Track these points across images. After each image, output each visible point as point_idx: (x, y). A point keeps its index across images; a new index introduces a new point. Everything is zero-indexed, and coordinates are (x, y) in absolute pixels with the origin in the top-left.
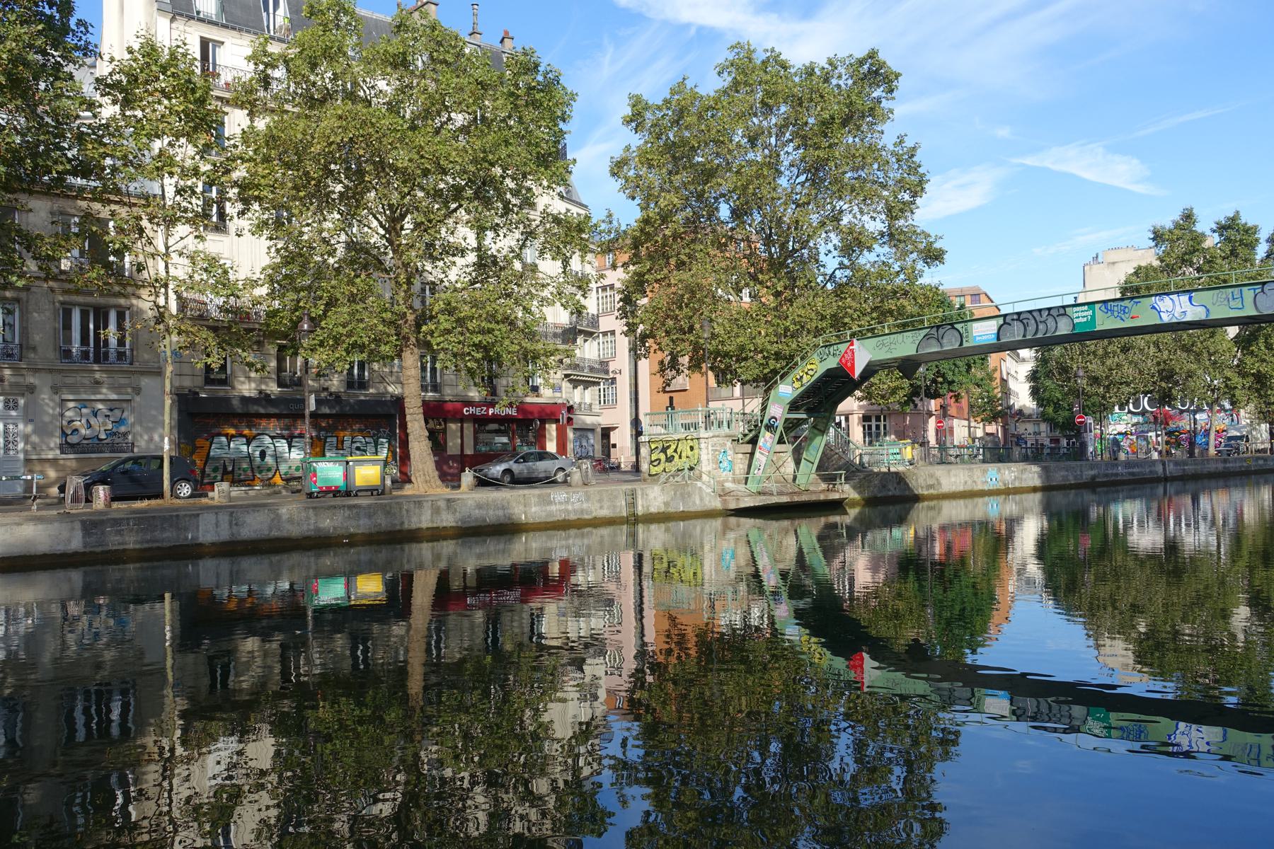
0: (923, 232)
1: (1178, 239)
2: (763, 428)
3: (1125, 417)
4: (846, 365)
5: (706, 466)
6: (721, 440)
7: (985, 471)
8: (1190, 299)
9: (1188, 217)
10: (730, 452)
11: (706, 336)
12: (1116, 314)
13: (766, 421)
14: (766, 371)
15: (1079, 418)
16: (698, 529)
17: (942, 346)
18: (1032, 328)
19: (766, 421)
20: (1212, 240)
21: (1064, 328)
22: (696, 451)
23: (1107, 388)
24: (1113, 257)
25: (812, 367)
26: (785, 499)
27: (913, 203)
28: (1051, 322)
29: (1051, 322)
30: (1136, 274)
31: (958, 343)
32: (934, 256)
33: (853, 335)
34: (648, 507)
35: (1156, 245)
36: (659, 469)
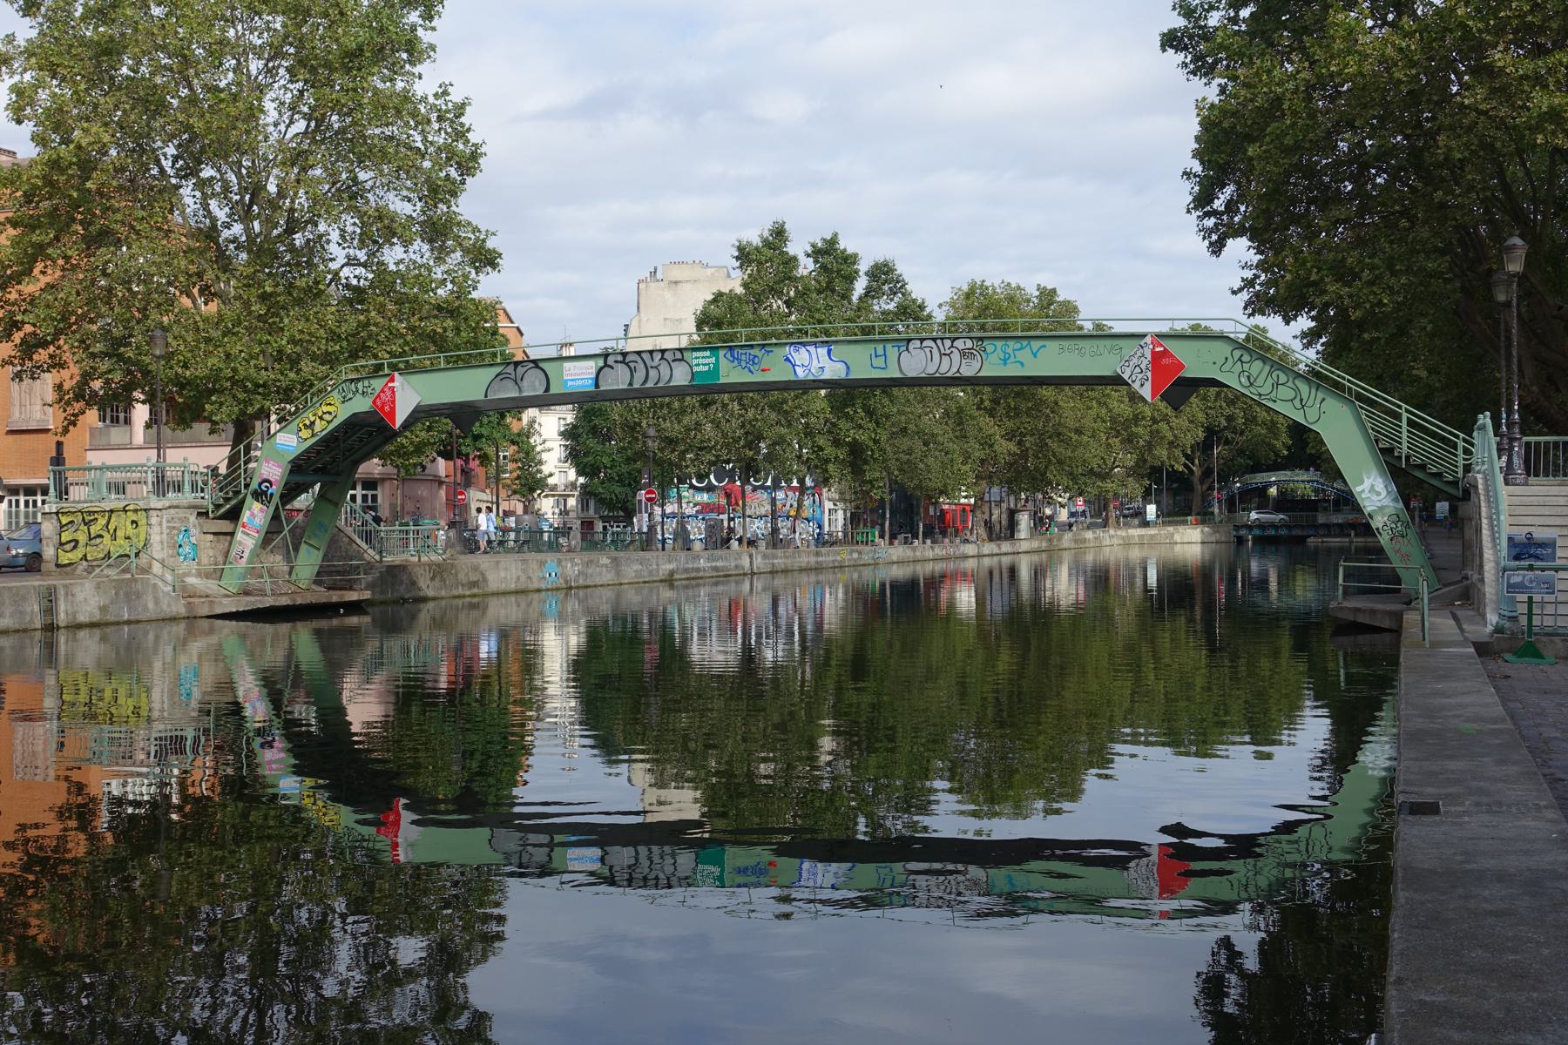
0: (469, 223)
1: (766, 262)
4: (382, 409)
5: (158, 550)
6: (181, 513)
7: (542, 563)
8: (829, 352)
9: (779, 233)
12: (743, 364)
16: (151, 636)
17: (520, 391)
20: (806, 267)
22: (142, 529)
24: (676, 273)
25: (329, 408)
26: (284, 601)
27: (463, 182)
30: (714, 301)
32: (485, 259)
34: (74, 614)
35: (741, 267)
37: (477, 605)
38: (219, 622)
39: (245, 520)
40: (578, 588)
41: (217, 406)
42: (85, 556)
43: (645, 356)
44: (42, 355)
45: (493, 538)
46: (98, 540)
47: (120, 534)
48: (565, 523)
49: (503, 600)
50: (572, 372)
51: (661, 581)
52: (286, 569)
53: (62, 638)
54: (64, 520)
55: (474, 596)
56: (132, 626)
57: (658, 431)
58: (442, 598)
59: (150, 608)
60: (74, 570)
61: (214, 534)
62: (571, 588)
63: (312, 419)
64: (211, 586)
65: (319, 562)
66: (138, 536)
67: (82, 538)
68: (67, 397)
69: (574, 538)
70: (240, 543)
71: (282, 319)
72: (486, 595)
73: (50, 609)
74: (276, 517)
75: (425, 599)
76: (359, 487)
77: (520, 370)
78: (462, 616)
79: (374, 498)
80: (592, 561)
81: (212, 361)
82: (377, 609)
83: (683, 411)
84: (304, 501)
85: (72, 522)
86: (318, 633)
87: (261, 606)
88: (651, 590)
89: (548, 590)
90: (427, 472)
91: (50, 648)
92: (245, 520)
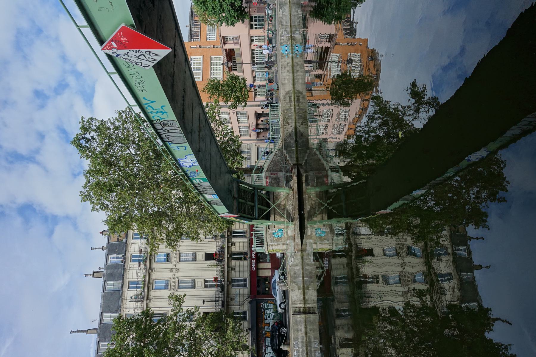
38: (304, 243)
58: (295, 118)
75: (296, 128)
76: (252, 23)
79: (256, 17)
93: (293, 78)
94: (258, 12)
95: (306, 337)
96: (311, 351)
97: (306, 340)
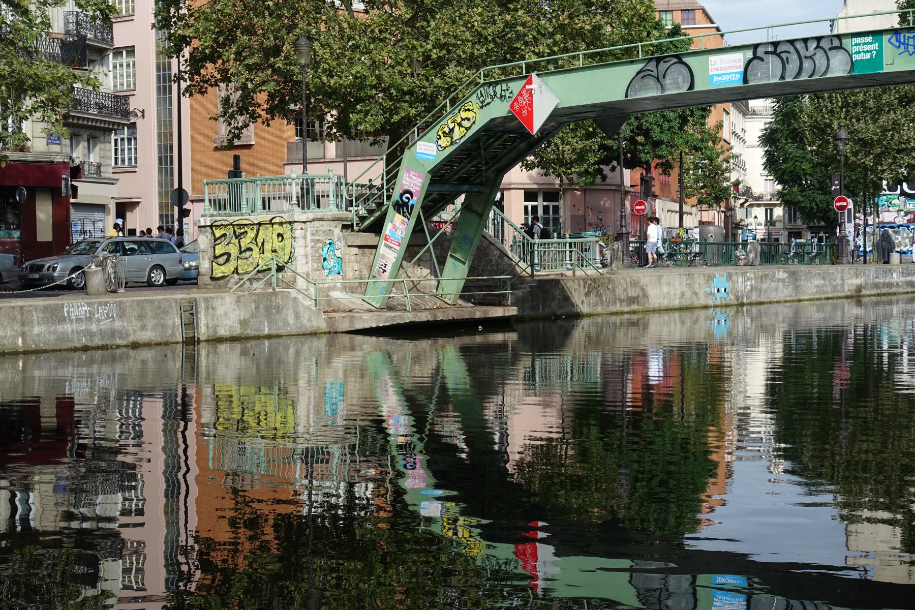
2: (391, 209)
3: (896, 201)
4: (520, 113)
5: (302, 265)
6: (326, 226)
7: (710, 278)
10: (339, 244)
11: (303, 61)
13: (396, 196)
14: (396, 118)
15: (839, 200)
16: (292, 351)
17: (663, 89)
18: (793, 67)
19: (396, 196)
21: (838, 68)
22: (288, 242)
23: (878, 159)
26: (424, 317)
28: (820, 59)
29: (820, 59)
31: (687, 86)
33: (530, 68)
36: (228, 269)
37: (638, 323)
38: (359, 338)
39: (387, 233)
40: (750, 304)
41: (362, 115)
42: (237, 269)
43: (799, 45)
44: (210, 69)
45: (662, 250)
46: (248, 254)
47: (268, 247)
48: (769, 234)
49: (666, 318)
50: (718, 66)
51: (847, 297)
52: (434, 283)
53: (203, 351)
54: (218, 233)
55: (634, 312)
56: (273, 341)
57: (851, 133)
58: (598, 315)
59: (290, 322)
60: (227, 283)
61: (360, 247)
62: (742, 305)
63: (451, 126)
64: (353, 300)
65: (465, 277)
66: (283, 249)
67: (234, 251)
68: (230, 111)
69: (752, 250)
70: (383, 257)
71: (428, 22)
72: (647, 312)
73: (191, 323)
74: (418, 230)
76: (540, 199)
77: (663, 66)
78: (620, 335)
79: (556, 209)
80: (766, 276)
81: (357, 68)
82: (527, 326)
83: (879, 111)
84: (449, 214)
85: (224, 235)
86: (465, 351)
87: (400, 322)
88: (835, 307)
89: (716, 306)
90: (608, 181)
91: (191, 360)
92: (387, 233)
93: (671, 310)
94: (572, 216)
95: (126, 346)
96: (91, 362)
97: (118, 347)
